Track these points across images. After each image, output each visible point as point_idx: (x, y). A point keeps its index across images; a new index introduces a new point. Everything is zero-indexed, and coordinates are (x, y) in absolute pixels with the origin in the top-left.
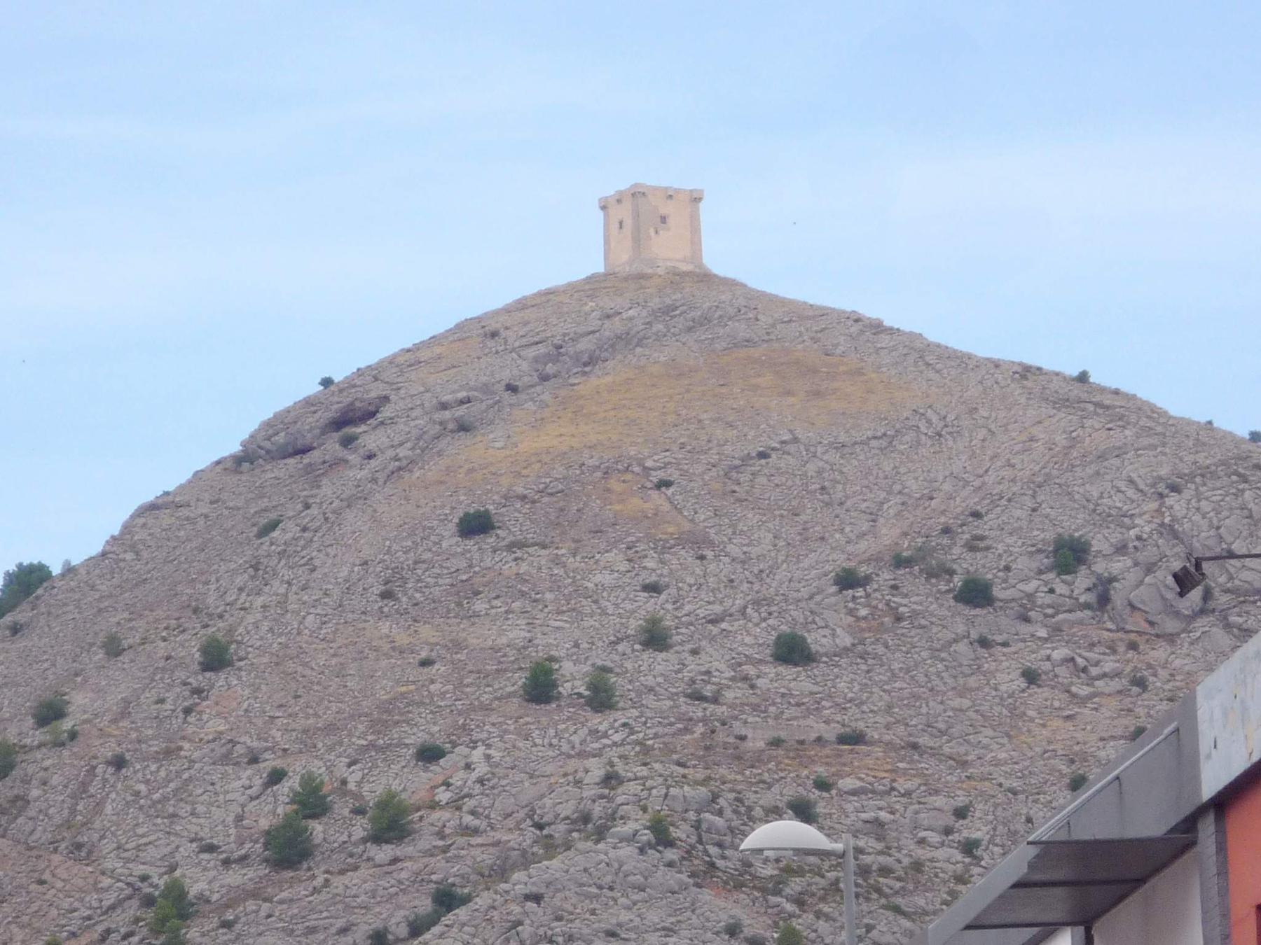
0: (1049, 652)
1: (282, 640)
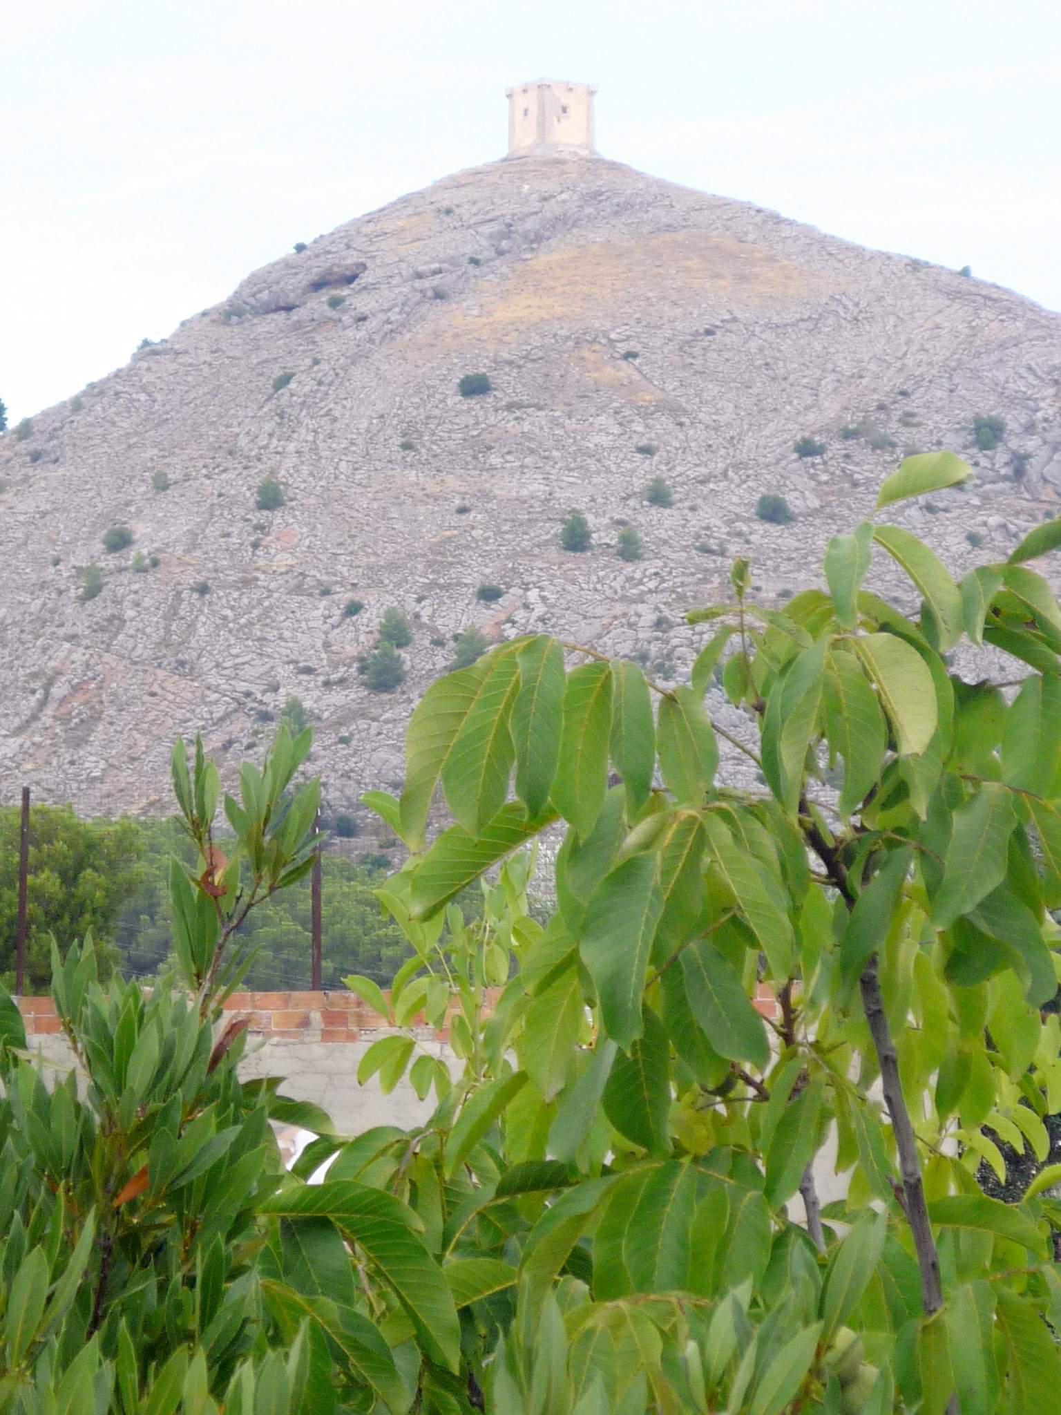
0: (985, 518)
1: (323, 483)
